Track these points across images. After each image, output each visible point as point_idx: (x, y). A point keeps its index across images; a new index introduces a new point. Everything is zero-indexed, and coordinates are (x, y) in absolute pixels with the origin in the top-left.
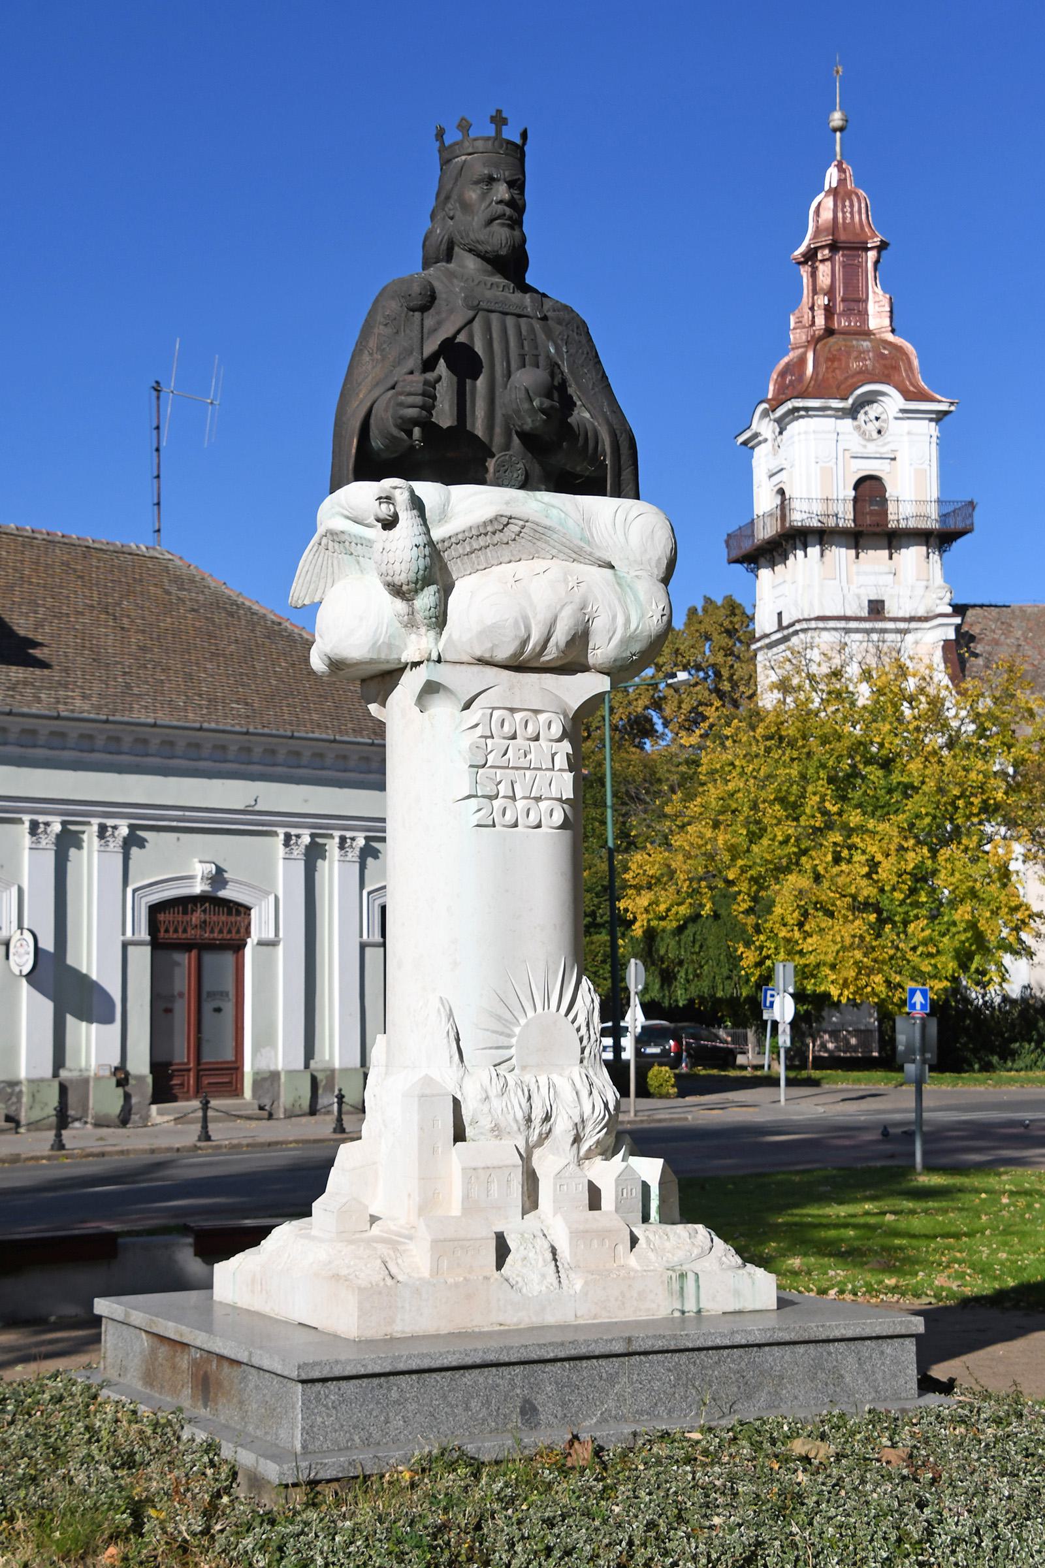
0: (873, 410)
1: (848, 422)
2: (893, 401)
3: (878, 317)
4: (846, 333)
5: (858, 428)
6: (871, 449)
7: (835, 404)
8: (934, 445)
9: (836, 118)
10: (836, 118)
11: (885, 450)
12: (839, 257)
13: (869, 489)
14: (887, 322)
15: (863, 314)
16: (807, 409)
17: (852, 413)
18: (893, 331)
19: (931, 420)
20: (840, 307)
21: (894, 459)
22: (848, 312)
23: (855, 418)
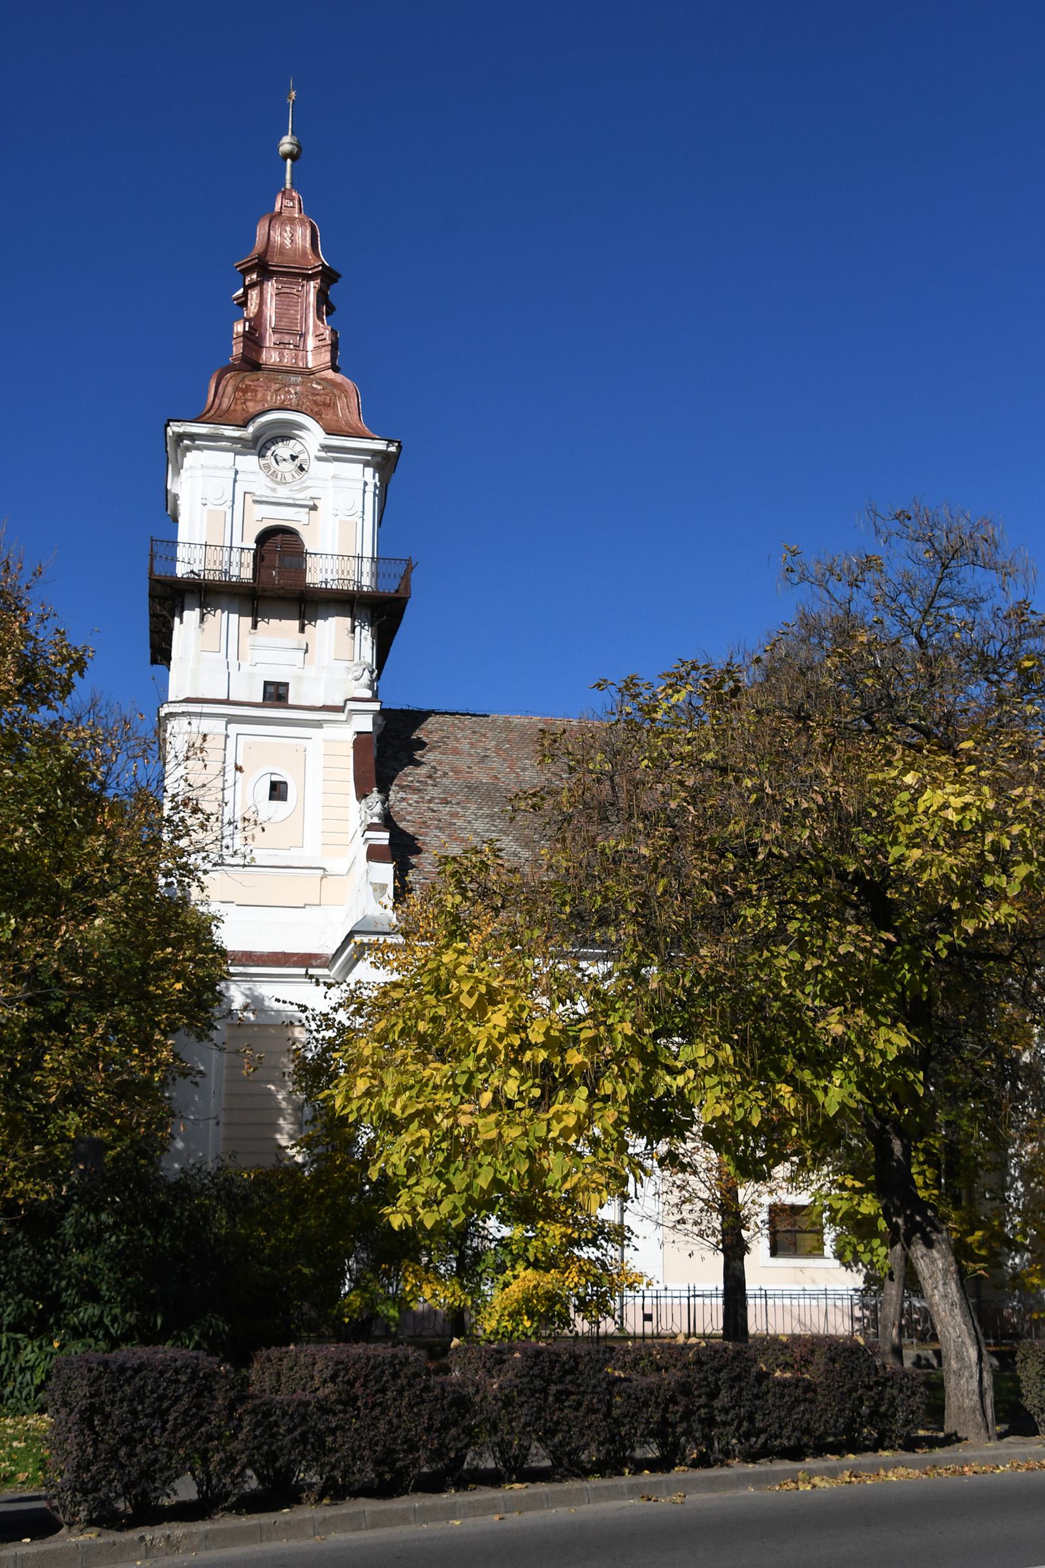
0: (283, 450)
1: (249, 463)
2: (313, 436)
3: (315, 355)
4: (277, 370)
5: (267, 467)
6: (283, 493)
7: (229, 431)
8: (369, 496)
9: (286, 144)
10: (286, 144)
11: (303, 497)
12: (271, 287)
13: (279, 545)
14: (326, 357)
15: (300, 348)
16: (192, 437)
17: (260, 445)
18: (335, 369)
19: (366, 464)
20: (270, 339)
21: (314, 508)
22: (281, 345)
23: (261, 455)
